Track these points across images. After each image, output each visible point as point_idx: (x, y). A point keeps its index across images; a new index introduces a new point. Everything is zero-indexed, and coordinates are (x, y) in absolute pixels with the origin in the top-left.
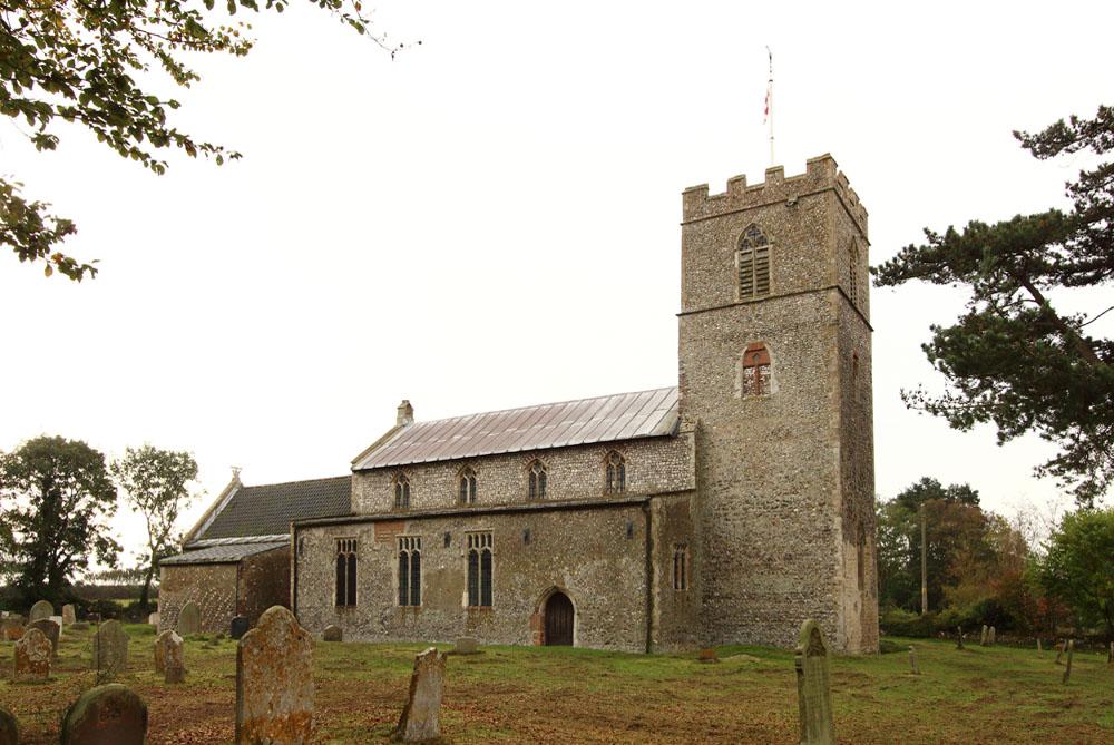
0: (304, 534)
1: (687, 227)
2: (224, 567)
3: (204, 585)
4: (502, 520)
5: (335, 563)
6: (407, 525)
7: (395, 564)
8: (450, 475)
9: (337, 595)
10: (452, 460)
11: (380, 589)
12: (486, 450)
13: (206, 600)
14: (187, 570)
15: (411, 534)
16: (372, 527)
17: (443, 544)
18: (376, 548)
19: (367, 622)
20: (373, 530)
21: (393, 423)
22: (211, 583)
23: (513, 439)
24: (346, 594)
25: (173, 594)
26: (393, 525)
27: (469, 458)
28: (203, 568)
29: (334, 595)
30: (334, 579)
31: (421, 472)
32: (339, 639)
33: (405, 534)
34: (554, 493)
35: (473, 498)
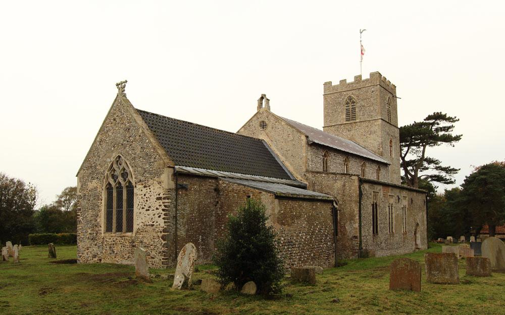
6: (390, 188)
13: (313, 232)
14: (296, 204)
21: (256, 111)
34: (382, 180)
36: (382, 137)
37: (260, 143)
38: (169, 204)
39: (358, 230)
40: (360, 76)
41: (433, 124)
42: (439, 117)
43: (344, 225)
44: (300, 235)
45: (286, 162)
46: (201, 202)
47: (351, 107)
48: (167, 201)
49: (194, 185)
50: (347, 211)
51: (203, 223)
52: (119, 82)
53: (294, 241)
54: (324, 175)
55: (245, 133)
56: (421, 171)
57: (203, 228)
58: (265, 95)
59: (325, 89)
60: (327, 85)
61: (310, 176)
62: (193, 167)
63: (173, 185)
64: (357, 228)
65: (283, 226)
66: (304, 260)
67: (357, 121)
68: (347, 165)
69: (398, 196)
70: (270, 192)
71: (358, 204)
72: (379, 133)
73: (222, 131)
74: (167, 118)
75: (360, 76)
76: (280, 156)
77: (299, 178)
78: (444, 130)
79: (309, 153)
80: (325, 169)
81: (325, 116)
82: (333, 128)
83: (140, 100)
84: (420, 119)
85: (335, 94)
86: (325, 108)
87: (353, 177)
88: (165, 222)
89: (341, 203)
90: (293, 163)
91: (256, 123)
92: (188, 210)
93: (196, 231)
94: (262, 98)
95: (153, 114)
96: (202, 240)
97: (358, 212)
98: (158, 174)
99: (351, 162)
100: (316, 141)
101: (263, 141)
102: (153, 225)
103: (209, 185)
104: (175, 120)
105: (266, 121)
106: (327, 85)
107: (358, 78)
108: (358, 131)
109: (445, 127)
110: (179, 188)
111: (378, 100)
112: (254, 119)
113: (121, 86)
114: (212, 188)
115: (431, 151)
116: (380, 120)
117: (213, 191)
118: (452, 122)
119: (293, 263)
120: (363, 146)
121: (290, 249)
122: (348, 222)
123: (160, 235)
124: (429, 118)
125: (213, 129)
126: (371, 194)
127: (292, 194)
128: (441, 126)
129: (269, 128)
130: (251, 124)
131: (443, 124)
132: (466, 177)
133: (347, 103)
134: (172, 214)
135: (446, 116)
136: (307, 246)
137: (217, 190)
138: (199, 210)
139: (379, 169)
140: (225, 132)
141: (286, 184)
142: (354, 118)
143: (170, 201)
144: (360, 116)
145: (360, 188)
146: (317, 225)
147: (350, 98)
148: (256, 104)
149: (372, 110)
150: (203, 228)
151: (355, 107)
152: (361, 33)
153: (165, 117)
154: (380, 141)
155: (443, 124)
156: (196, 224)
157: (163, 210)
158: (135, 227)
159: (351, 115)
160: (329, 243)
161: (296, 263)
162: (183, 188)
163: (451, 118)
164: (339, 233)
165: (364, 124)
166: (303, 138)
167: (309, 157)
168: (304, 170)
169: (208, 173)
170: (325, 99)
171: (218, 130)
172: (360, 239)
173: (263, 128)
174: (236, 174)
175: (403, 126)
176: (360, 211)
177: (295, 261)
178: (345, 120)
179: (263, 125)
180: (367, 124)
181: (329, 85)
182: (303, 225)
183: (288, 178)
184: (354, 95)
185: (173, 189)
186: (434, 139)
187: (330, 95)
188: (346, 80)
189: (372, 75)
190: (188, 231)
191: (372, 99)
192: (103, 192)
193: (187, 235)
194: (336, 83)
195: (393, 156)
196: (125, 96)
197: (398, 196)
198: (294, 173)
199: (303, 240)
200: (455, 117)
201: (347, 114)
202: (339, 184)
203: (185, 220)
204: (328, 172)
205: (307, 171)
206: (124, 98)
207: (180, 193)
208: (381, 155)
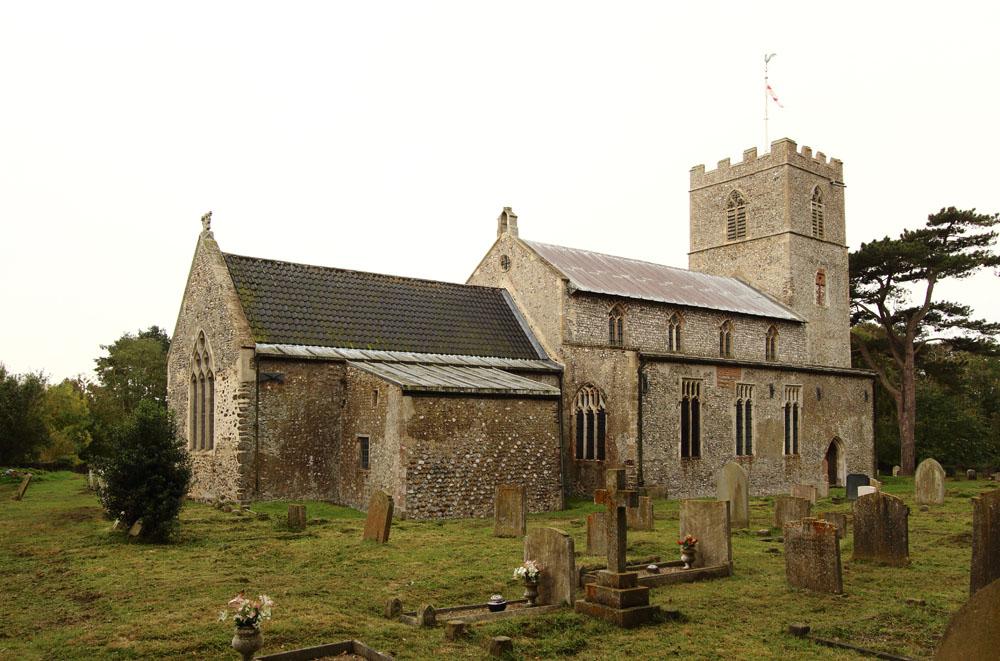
0: (648, 369)
1: (777, 184)
2: (530, 403)
3: (493, 432)
4: (805, 377)
5: (680, 408)
6: (743, 372)
7: (733, 412)
8: (660, 319)
9: (682, 445)
10: (717, 312)
11: (721, 437)
12: (658, 295)
13: (502, 454)
14: (461, 404)
15: (744, 382)
16: (714, 370)
17: (768, 395)
18: (717, 394)
19: (711, 474)
20: (715, 373)
21: (495, 239)
22: (510, 428)
23: (723, 300)
24: (691, 447)
25: (432, 444)
26: (732, 372)
27: (646, 301)
28: (492, 404)
29: (680, 444)
30: (679, 426)
31: (637, 310)
32: (666, 496)
33: (741, 382)
34: (782, 358)
35: (678, 347)
36: (792, 268)
37: (497, 293)
38: (246, 406)
39: (635, 451)
40: (754, 150)
41: (950, 230)
42: (952, 216)
43: (614, 439)
44: (468, 456)
45: (536, 328)
46: (313, 401)
47: (736, 212)
48: (242, 401)
49: (297, 375)
50: (618, 414)
51: (317, 435)
52: (203, 215)
53: (451, 467)
54: (587, 350)
55: (481, 282)
56: (939, 330)
57: (318, 443)
58: (509, 209)
59: (692, 180)
60: (697, 171)
61: (568, 351)
62: (332, 347)
63: (252, 376)
64: (632, 447)
65: (424, 442)
66: (477, 499)
67: (748, 238)
68: (678, 328)
69: (771, 386)
70: (397, 384)
71: (637, 402)
72: (786, 260)
73: (409, 279)
74: (294, 265)
75: (754, 150)
76: (528, 316)
77: (553, 355)
78: (978, 243)
79: (572, 311)
80: (616, 337)
81: (692, 233)
82: (705, 255)
83: (238, 240)
84: (919, 224)
85: (710, 189)
86: (693, 217)
87: (628, 354)
88: (240, 434)
89: (609, 399)
90: (544, 327)
91: (496, 260)
92: (284, 414)
93: (302, 449)
94: (504, 214)
95: (266, 261)
96: (315, 462)
97: (636, 418)
98: (232, 360)
99: (688, 323)
100: (584, 288)
101: (503, 293)
102: (230, 439)
103: (321, 376)
104: (309, 267)
105: (509, 255)
106: (697, 171)
107: (751, 155)
108: (748, 259)
109: (976, 237)
110: (262, 381)
111: (785, 195)
112: (494, 252)
113: (206, 219)
114: (336, 378)
115: (948, 289)
116: (788, 235)
117: (339, 384)
118: (986, 225)
119: (449, 503)
120: (757, 288)
121: (440, 480)
122: (620, 435)
123: (236, 453)
124: (934, 220)
125: (388, 277)
126: (677, 383)
127: (444, 388)
128: (966, 235)
129: (514, 268)
130: (490, 261)
131: (971, 230)
132: (96, 370)
133: (731, 205)
134: (251, 421)
135: (974, 213)
136: (486, 476)
137: (344, 382)
138: (309, 415)
139: (773, 333)
140: (415, 280)
141: (503, 369)
142: (742, 234)
143: (247, 400)
144: (752, 229)
145: (640, 372)
146: (515, 440)
147: (735, 195)
148: (495, 225)
149: (775, 217)
150: (318, 443)
151: (743, 211)
152: (767, 62)
153: (289, 264)
154: (788, 276)
155: (971, 230)
156: (302, 438)
157: (239, 415)
158: (215, 445)
159: (737, 229)
160: (546, 472)
161: (455, 503)
162: (273, 379)
163: (987, 217)
164: (607, 455)
165: (759, 245)
166: (559, 283)
167: (573, 317)
168: (560, 341)
169: (336, 355)
170: (692, 199)
171: (400, 278)
172: (641, 466)
173: (506, 268)
174: (403, 354)
175: (880, 239)
176: (640, 415)
177: (453, 500)
178: (726, 238)
179: (506, 263)
180: (765, 241)
181: (699, 172)
182: (478, 440)
183: (534, 356)
184: (742, 188)
185: (253, 382)
186: (931, 263)
187: (700, 191)
188: (729, 159)
189: (775, 146)
190: (284, 447)
191: (774, 194)
192: (189, 387)
193: (282, 454)
194: (711, 166)
195: (827, 304)
196: (210, 236)
197: (771, 386)
198: (546, 347)
199: (475, 465)
200: (997, 215)
201: (731, 226)
202: (607, 366)
203: (278, 430)
204: (625, 344)
205: (566, 343)
206: (210, 239)
207: (269, 387)
208: (790, 303)
